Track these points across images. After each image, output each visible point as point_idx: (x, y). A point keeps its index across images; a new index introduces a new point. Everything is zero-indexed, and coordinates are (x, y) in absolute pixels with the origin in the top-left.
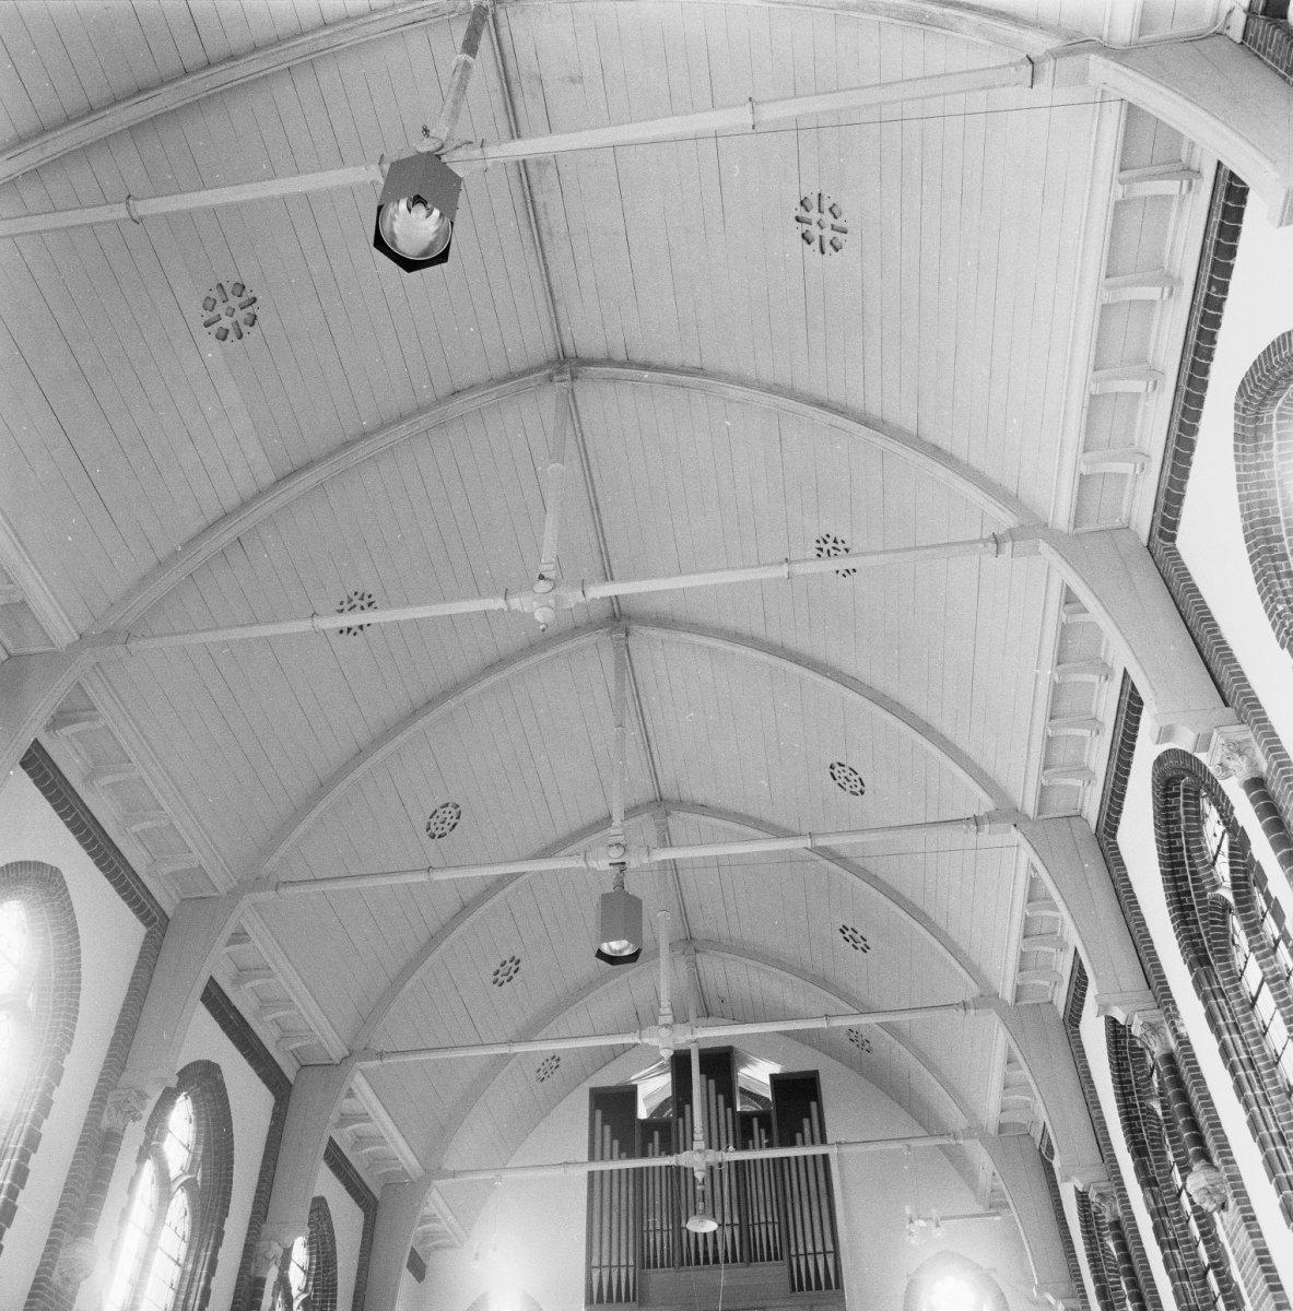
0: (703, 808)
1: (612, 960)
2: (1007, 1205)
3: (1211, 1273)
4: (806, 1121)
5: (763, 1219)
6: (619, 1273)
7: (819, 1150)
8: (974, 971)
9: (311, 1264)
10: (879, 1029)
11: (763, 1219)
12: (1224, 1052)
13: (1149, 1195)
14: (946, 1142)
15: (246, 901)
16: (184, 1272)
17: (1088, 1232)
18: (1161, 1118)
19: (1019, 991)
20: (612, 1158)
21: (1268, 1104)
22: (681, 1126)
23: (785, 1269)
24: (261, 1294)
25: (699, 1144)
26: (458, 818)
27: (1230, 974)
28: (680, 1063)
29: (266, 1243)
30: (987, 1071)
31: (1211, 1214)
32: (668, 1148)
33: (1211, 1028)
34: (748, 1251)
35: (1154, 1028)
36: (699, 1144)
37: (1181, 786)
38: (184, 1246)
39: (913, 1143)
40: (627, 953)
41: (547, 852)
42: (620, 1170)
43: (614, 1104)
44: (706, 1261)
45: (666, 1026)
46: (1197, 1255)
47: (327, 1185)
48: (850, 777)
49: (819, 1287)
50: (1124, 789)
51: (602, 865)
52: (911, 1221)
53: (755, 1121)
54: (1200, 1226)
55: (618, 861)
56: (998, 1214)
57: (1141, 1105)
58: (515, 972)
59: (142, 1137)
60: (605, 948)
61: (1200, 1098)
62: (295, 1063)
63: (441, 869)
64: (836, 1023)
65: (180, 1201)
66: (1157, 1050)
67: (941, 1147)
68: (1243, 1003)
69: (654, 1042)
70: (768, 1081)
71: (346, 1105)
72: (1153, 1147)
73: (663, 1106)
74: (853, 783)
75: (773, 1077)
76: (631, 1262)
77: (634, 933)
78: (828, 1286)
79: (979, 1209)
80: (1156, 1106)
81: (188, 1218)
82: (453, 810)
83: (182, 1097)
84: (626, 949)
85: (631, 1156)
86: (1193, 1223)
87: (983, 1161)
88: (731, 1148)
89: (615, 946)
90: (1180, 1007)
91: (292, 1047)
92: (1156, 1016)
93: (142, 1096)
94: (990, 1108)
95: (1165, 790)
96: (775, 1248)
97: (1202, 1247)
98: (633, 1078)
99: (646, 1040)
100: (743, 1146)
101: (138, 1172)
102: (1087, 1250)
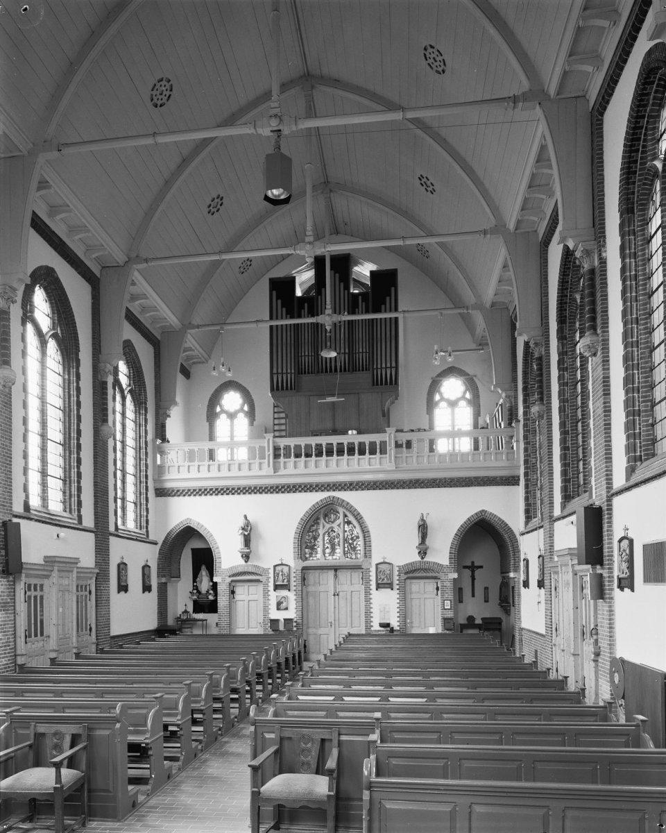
0: (336, 83)
1: (275, 202)
2: (487, 344)
3: (579, 383)
4: (388, 298)
5: (361, 350)
6: (282, 377)
7: (393, 315)
8: (495, 210)
9: (130, 373)
10: (436, 245)
11: (361, 350)
12: (623, 270)
13: (560, 345)
14: (462, 311)
15: (41, 159)
16: (64, 379)
17: (526, 360)
18: (579, 304)
19: (519, 223)
20: (282, 318)
21: (637, 301)
22: (320, 299)
23: (371, 375)
24: (106, 389)
25: (328, 311)
26: (171, 90)
27: (644, 220)
28: (319, 263)
29: (103, 364)
30: (490, 272)
31: (588, 358)
32: (313, 312)
33: (621, 254)
34: (351, 366)
35: (588, 253)
36: (328, 311)
37: (658, 76)
38: (61, 367)
39: (444, 312)
40: (282, 197)
41: (230, 121)
42: (286, 325)
43: (282, 287)
44: (331, 371)
45: (310, 243)
46: (575, 375)
47: (129, 333)
48: (433, 61)
49: (386, 384)
50: (619, 75)
51: (266, 132)
52: (437, 353)
53: (360, 297)
54: (581, 362)
55: (275, 129)
56: (482, 349)
57: (571, 296)
58: (221, 205)
59: (20, 313)
60: (269, 194)
61: (601, 296)
62: (99, 267)
63: (165, 134)
64: (408, 242)
65: (52, 345)
66: (586, 266)
67: (460, 313)
68: (644, 239)
69: (302, 253)
70: (368, 274)
71: (133, 289)
72: (570, 319)
73: (310, 289)
74: (438, 63)
75: (372, 272)
76: (293, 371)
77: (286, 186)
78: (391, 383)
79: (473, 346)
80: (578, 297)
81: (59, 353)
82: (166, 83)
83: (37, 288)
84: (282, 194)
85: (292, 317)
86: (578, 359)
87: (479, 320)
88: (346, 313)
89: (275, 193)
90: (607, 240)
91: (94, 256)
92: (592, 245)
93: (14, 290)
94: (489, 292)
95: (646, 78)
96: (366, 365)
97: (579, 371)
98: (293, 272)
99: (298, 252)
100: (352, 311)
101: (24, 330)
102: (523, 368)
